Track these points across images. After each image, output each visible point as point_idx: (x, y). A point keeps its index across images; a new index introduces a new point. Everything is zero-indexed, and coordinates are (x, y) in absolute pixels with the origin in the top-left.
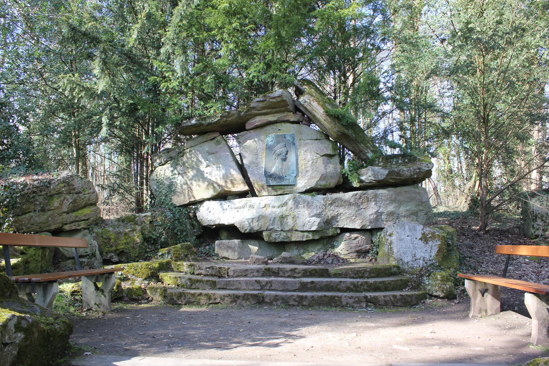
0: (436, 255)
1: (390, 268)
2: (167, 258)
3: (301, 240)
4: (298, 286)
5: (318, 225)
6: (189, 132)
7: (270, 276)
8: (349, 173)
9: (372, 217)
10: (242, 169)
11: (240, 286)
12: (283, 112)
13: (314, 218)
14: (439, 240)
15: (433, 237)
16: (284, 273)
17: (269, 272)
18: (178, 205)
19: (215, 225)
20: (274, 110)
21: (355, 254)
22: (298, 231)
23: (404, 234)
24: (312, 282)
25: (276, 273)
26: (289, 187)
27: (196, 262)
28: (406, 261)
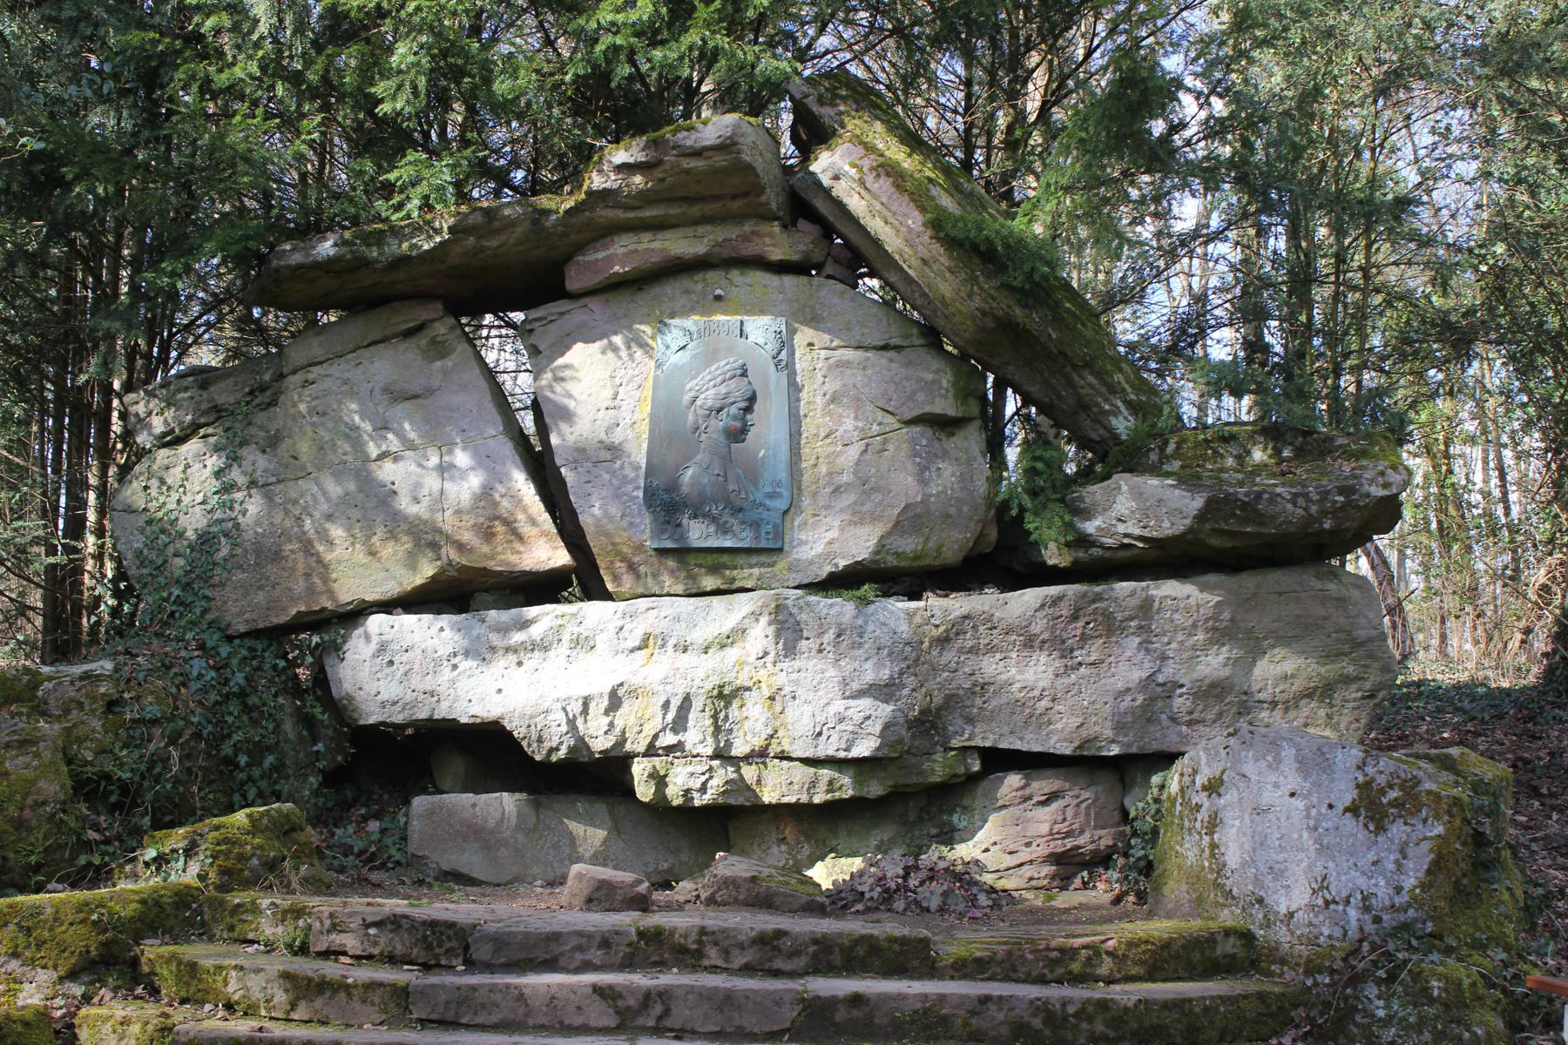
0: (1422, 886)
1: (1211, 939)
2: (186, 874)
3: (804, 799)
4: (790, 1014)
5: (882, 735)
6: (308, 292)
7: (662, 965)
8: (1027, 501)
9: (1126, 703)
10: (542, 468)
11: (521, 1011)
12: (738, 218)
13: (865, 703)
14: (1437, 817)
15: (1410, 801)
16: (726, 953)
17: (654, 948)
18: (242, 629)
19: (414, 723)
20: (696, 210)
21: (1047, 870)
22: (790, 759)
23: (1276, 786)
24: (856, 1000)
25: (687, 954)
26: (754, 560)
27: (318, 893)
28: (1283, 910)
